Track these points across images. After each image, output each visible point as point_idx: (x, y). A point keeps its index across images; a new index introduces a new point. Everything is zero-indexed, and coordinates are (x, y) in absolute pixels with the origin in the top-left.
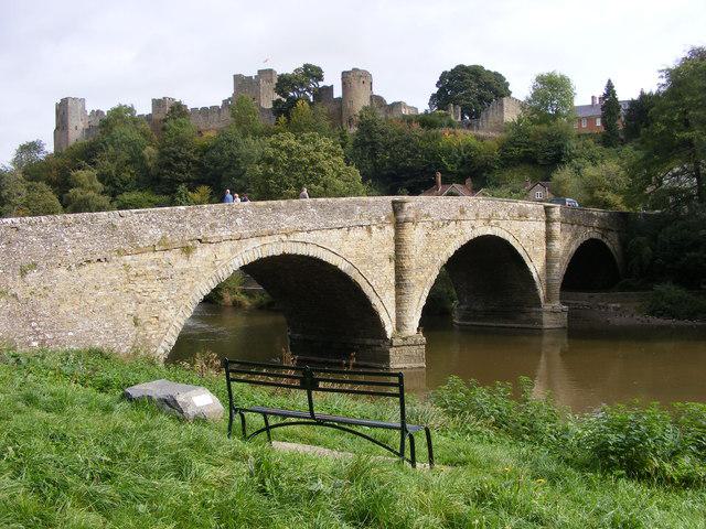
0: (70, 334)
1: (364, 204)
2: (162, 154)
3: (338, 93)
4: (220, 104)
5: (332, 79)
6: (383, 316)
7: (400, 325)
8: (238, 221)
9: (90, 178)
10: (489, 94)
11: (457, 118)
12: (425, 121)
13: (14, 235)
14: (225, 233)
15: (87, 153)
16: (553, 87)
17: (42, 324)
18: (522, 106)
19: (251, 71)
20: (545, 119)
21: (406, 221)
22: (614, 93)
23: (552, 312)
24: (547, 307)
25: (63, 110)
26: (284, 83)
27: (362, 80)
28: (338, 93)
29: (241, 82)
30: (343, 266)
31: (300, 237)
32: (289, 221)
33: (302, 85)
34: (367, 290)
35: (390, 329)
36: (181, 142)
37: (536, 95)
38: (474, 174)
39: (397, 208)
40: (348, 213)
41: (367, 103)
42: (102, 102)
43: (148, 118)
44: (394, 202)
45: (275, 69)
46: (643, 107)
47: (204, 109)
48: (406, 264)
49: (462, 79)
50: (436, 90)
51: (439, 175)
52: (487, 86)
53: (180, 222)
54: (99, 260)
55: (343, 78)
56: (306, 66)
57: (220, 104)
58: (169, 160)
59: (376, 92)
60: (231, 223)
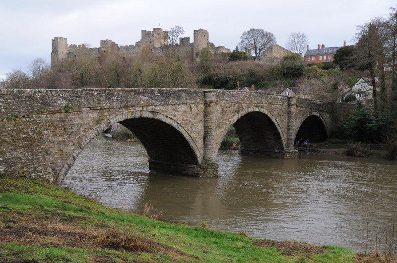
3: (192, 41)
4: (134, 44)
19: (150, 29)
21: (211, 102)
25: (55, 42)
29: (145, 34)
30: (175, 125)
38: (256, 81)
41: (205, 46)
43: (99, 49)
48: (209, 124)
53: (77, 97)
55: (194, 33)
57: (134, 44)
59: (210, 41)
60: (110, 99)
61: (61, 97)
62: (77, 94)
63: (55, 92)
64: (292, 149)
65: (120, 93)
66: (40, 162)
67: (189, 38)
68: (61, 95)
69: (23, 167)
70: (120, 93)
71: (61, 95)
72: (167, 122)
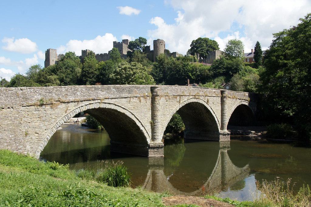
2: (83, 71)
3: (152, 49)
4: (107, 53)
5: (150, 43)
8: (78, 93)
10: (211, 50)
11: (197, 58)
12: (185, 59)
14: (72, 99)
16: (235, 44)
18: (222, 53)
20: (231, 58)
22: (260, 47)
23: (225, 138)
25: (48, 53)
26: (132, 45)
27: (161, 43)
28: (152, 49)
31: (106, 101)
35: (149, 140)
37: (227, 50)
40: (130, 92)
44: (151, 88)
45: (128, 39)
47: (101, 54)
49: (200, 43)
50: (190, 48)
52: (211, 46)
53: (50, 93)
54: (8, 108)
55: (154, 43)
57: (107, 53)
60: (75, 94)
61: (37, 93)
62: (49, 91)
63: (32, 89)
64: (226, 131)
65: (83, 89)
66: (21, 142)
67: (115, 43)
68: (38, 92)
69: (8, 146)
70: (83, 89)
71: (38, 92)
72: (90, 108)
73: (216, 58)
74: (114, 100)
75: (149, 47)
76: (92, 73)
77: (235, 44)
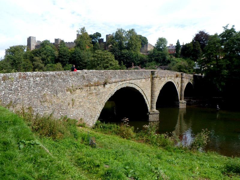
0: (72, 115)
1: (145, 72)
6: (148, 106)
7: (152, 107)
9: (39, 59)
13: (53, 79)
14: (114, 80)
15: (36, 53)
17: (63, 112)
20: (161, 50)
22: (179, 43)
24: (180, 101)
25: (29, 40)
31: (131, 81)
32: (129, 76)
33: (96, 38)
34: (145, 98)
36: (65, 51)
39: (153, 73)
40: (141, 75)
42: (41, 38)
43: (54, 44)
44: (152, 71)
46: (186, 47)
47: (69, 42)
51: (133, 64)
53: (102, 76)
56: (97, 33)
58: (61, 55)
73: (32, 49)
74: (134, 81)
75: (102, 40)
76: (66, 55)
77: (162, 41)
